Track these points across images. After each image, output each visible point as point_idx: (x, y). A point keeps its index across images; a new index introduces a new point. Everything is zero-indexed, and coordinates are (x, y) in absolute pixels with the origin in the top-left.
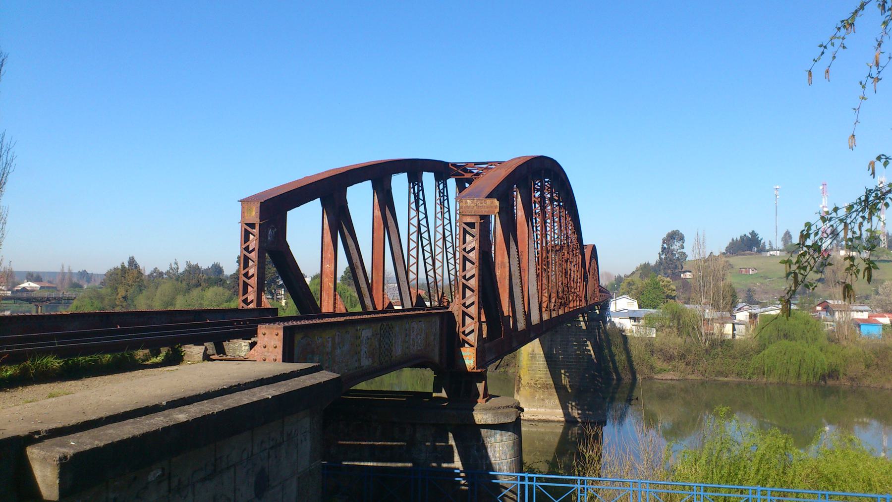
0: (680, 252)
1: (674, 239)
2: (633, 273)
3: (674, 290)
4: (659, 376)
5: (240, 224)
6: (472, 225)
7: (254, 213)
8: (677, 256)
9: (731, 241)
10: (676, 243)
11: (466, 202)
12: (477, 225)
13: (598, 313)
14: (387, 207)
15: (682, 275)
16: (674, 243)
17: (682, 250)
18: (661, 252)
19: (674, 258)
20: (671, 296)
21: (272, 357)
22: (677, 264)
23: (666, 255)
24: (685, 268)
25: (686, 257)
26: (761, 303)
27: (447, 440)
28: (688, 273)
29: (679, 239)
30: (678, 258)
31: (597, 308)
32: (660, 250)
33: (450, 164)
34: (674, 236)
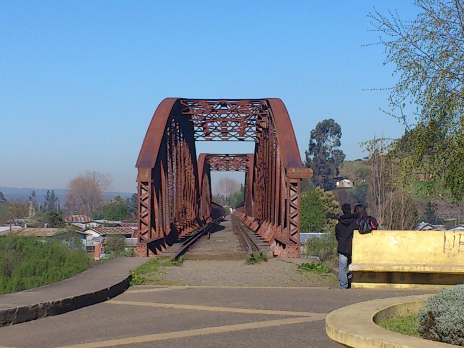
0: (335, 151)
1: (327, 131)
3: (337, 207)
5: (137, 183)
7: (147, 176)
8: (331, 156)
10: (329, 137)
11: (292, 170)
15: (338, 183)
16: (326, 137)
18: (308, 151)
19: (327, 159)
20: (333, 214)
21: (292, 256)
22: (330, 167)
23: (315, 155)
24: (343, 172)
25: (344, 157)
26: (445, 222)
28: (346, 180)
29: (333, 132)
30: (332, 158)
33: (181, 101)
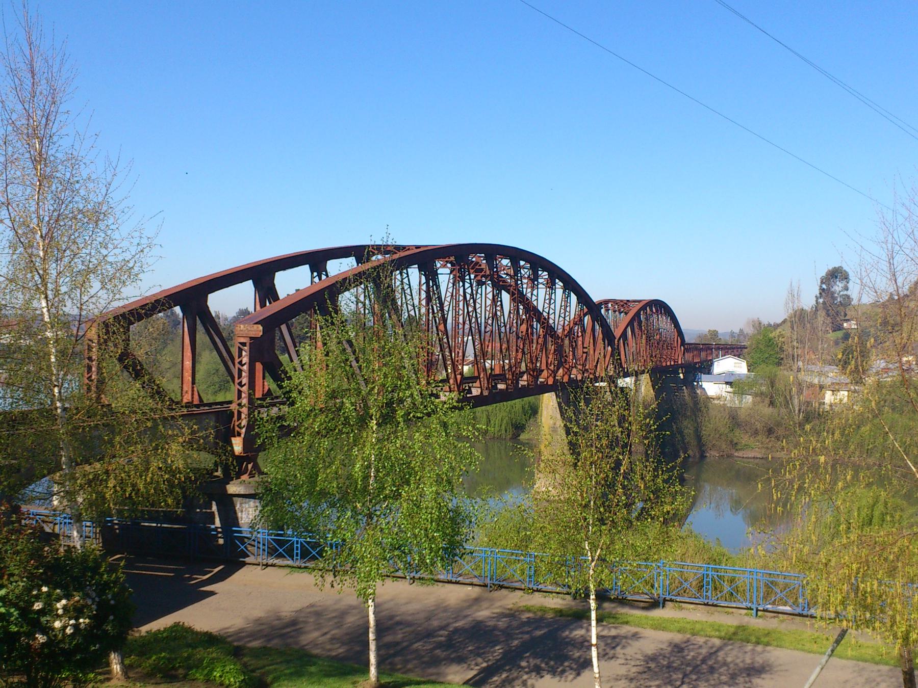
1: (836, 277)
4: (740, 454)
6: (244, 344)
8: (839, 300)
9: (808, 299)
10: (838, 283)
12: (248, 344)
14: (198, 318)
15: (845, 325)
17: (845, 293)
31: (680, 371)
32: (817, 293)
34: (836, 274)
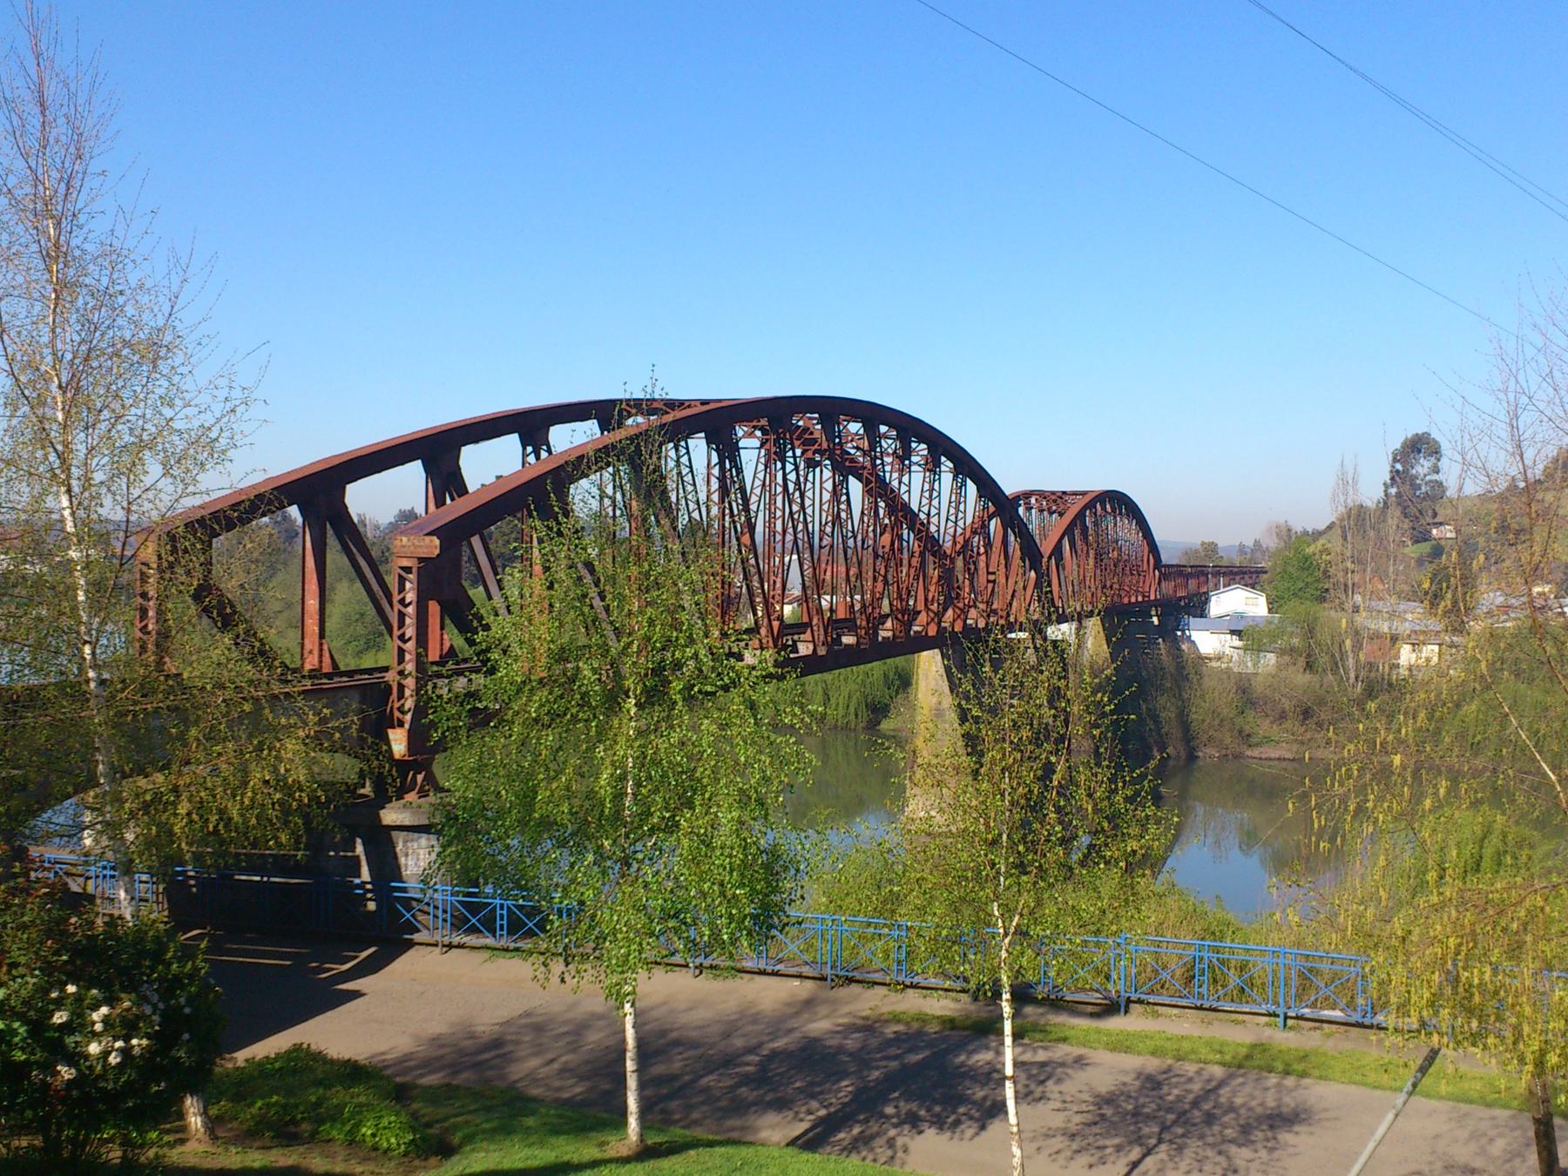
0: (1431, 481)
1: (1419, 451)
2: (1330, 527)
6: (408, 570)
8: (1423, 489)
9: (1372, 488)
10: (1422, 460)
12: (414, 570)
13: (1156, 622)
15: (1434, 531)
27: (353, 849)
32: (1387, 478)
34: (1419, 446)
